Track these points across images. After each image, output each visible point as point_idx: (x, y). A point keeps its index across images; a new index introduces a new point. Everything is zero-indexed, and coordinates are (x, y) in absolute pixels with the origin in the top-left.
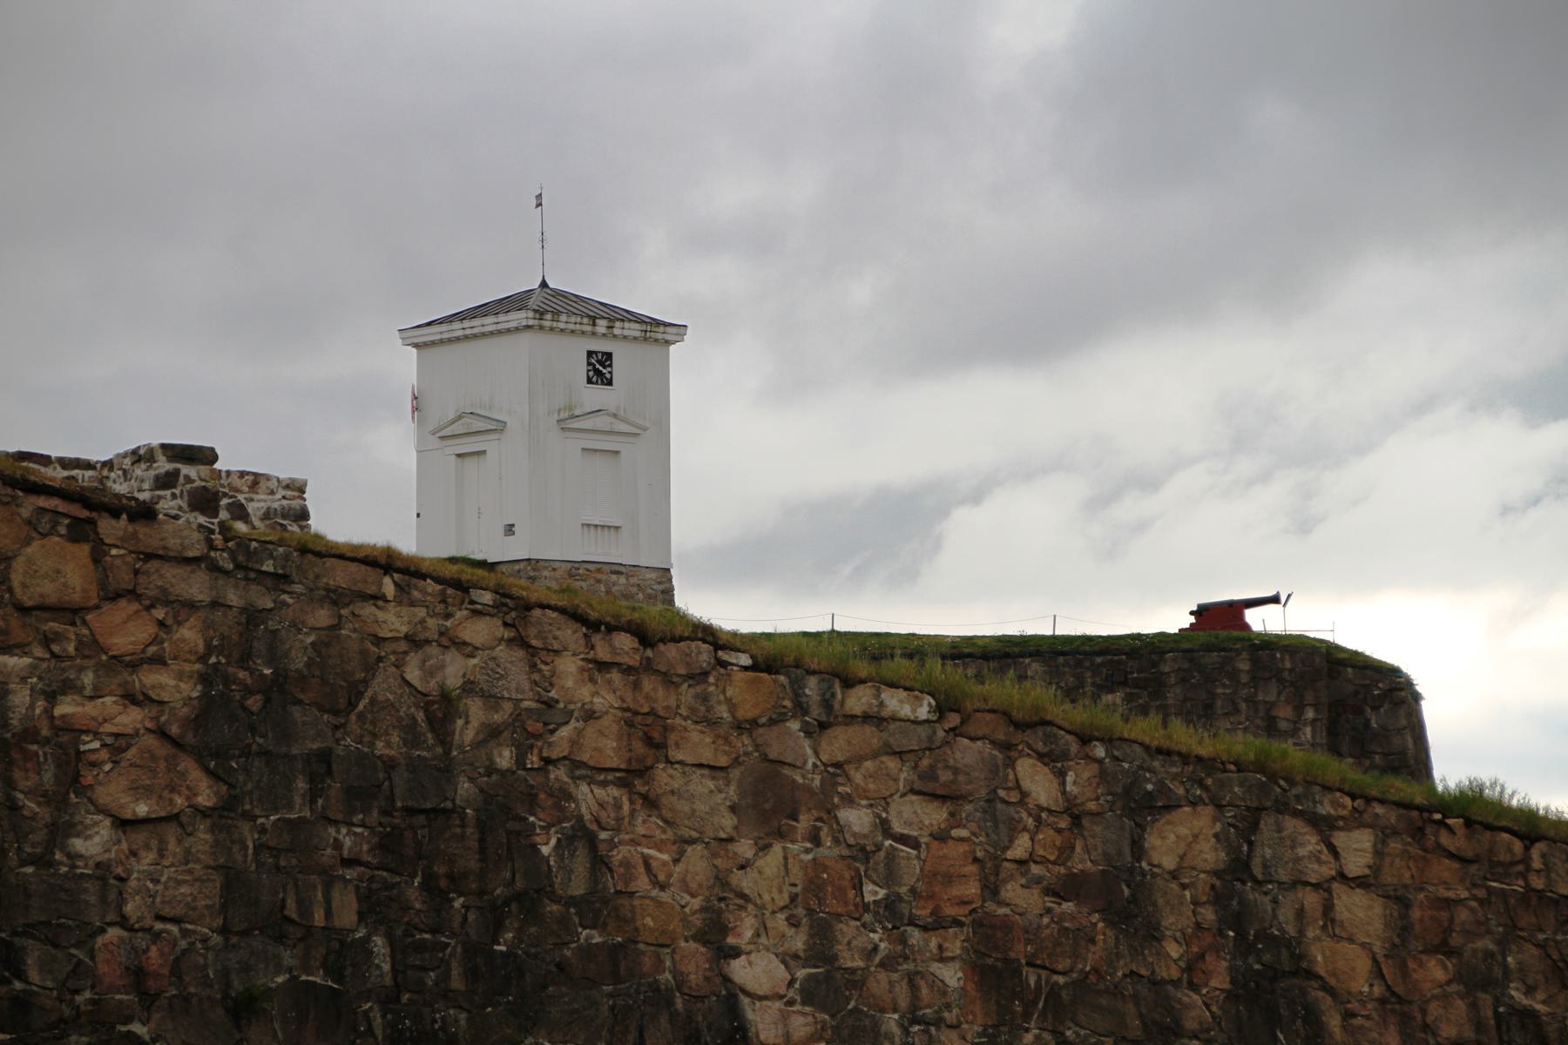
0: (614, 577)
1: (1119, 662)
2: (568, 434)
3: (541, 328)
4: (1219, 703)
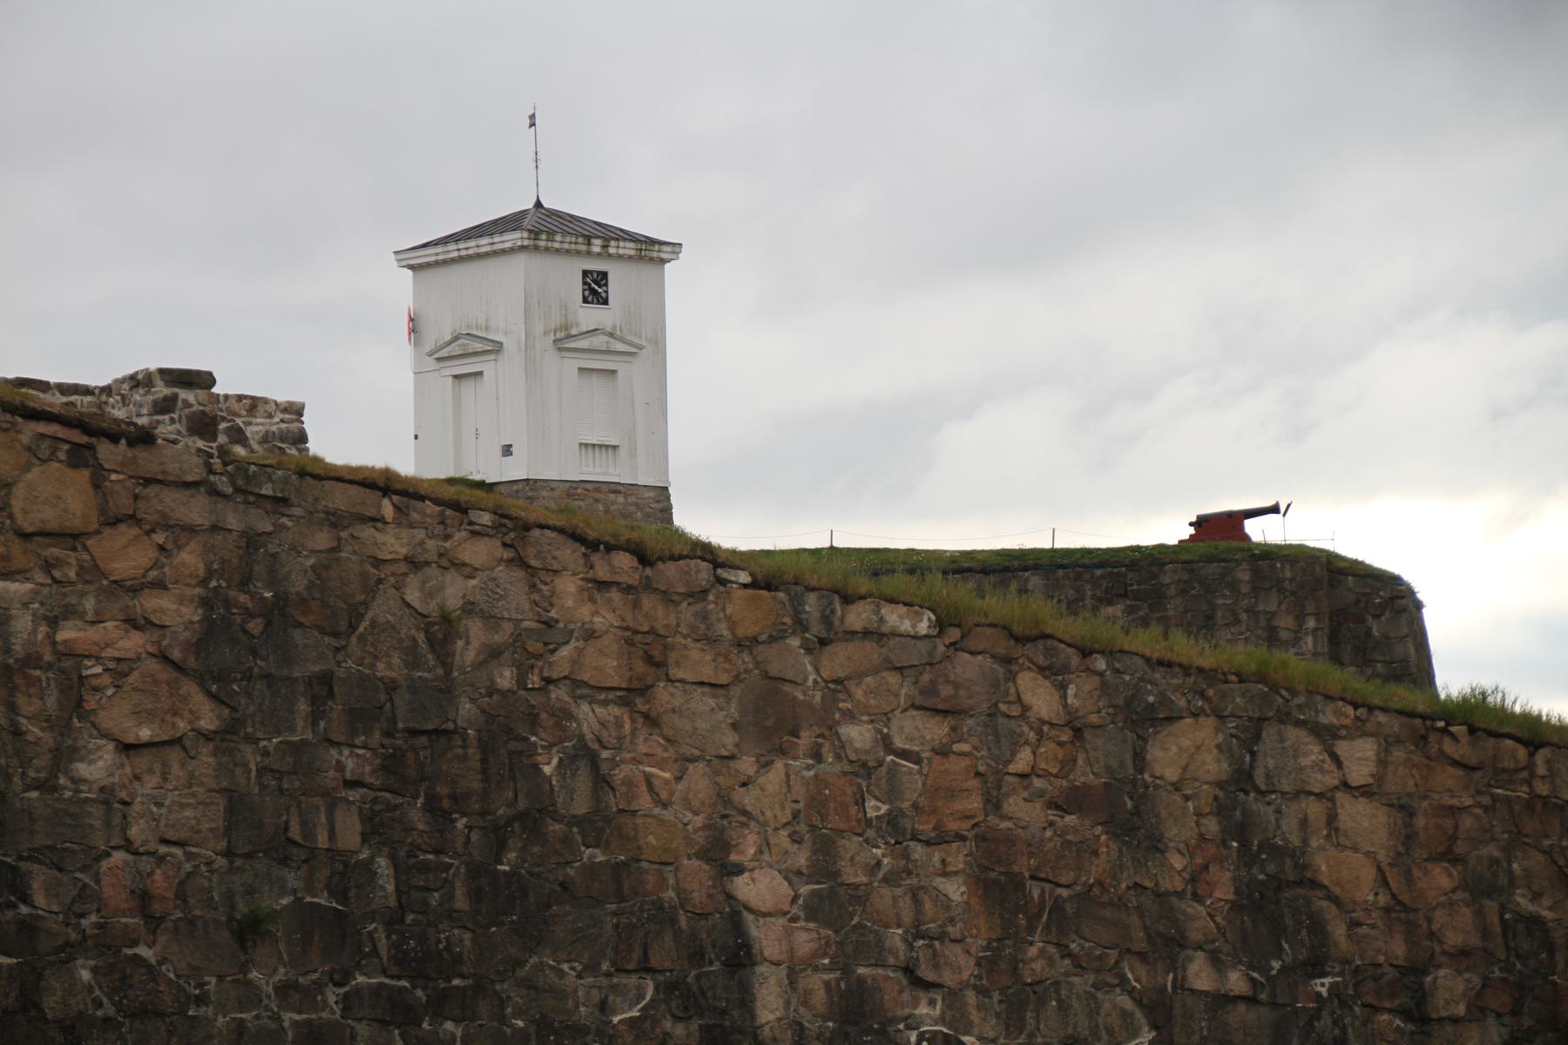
0: (612, 496)
1: (1118, 574)
2: (565, 354)
3: (536, 248)
4: (1219, 614)
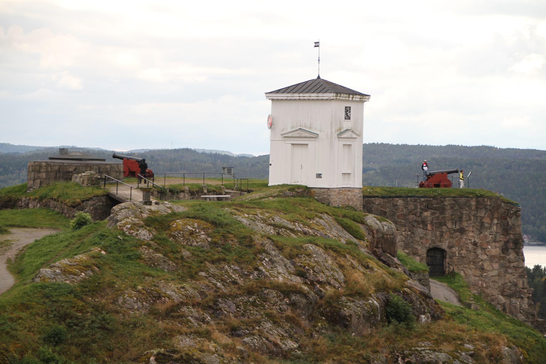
1: (430, 201)
2: (341, 140)
3: (336, 99)
4: (464, 216)
